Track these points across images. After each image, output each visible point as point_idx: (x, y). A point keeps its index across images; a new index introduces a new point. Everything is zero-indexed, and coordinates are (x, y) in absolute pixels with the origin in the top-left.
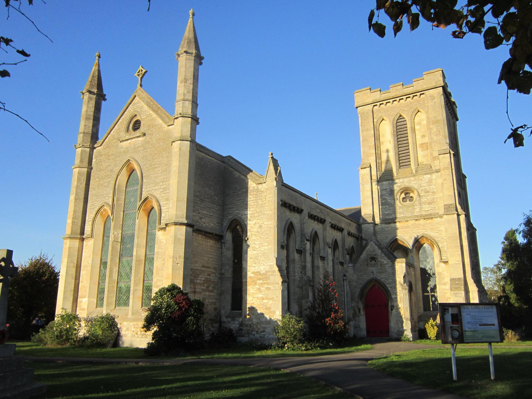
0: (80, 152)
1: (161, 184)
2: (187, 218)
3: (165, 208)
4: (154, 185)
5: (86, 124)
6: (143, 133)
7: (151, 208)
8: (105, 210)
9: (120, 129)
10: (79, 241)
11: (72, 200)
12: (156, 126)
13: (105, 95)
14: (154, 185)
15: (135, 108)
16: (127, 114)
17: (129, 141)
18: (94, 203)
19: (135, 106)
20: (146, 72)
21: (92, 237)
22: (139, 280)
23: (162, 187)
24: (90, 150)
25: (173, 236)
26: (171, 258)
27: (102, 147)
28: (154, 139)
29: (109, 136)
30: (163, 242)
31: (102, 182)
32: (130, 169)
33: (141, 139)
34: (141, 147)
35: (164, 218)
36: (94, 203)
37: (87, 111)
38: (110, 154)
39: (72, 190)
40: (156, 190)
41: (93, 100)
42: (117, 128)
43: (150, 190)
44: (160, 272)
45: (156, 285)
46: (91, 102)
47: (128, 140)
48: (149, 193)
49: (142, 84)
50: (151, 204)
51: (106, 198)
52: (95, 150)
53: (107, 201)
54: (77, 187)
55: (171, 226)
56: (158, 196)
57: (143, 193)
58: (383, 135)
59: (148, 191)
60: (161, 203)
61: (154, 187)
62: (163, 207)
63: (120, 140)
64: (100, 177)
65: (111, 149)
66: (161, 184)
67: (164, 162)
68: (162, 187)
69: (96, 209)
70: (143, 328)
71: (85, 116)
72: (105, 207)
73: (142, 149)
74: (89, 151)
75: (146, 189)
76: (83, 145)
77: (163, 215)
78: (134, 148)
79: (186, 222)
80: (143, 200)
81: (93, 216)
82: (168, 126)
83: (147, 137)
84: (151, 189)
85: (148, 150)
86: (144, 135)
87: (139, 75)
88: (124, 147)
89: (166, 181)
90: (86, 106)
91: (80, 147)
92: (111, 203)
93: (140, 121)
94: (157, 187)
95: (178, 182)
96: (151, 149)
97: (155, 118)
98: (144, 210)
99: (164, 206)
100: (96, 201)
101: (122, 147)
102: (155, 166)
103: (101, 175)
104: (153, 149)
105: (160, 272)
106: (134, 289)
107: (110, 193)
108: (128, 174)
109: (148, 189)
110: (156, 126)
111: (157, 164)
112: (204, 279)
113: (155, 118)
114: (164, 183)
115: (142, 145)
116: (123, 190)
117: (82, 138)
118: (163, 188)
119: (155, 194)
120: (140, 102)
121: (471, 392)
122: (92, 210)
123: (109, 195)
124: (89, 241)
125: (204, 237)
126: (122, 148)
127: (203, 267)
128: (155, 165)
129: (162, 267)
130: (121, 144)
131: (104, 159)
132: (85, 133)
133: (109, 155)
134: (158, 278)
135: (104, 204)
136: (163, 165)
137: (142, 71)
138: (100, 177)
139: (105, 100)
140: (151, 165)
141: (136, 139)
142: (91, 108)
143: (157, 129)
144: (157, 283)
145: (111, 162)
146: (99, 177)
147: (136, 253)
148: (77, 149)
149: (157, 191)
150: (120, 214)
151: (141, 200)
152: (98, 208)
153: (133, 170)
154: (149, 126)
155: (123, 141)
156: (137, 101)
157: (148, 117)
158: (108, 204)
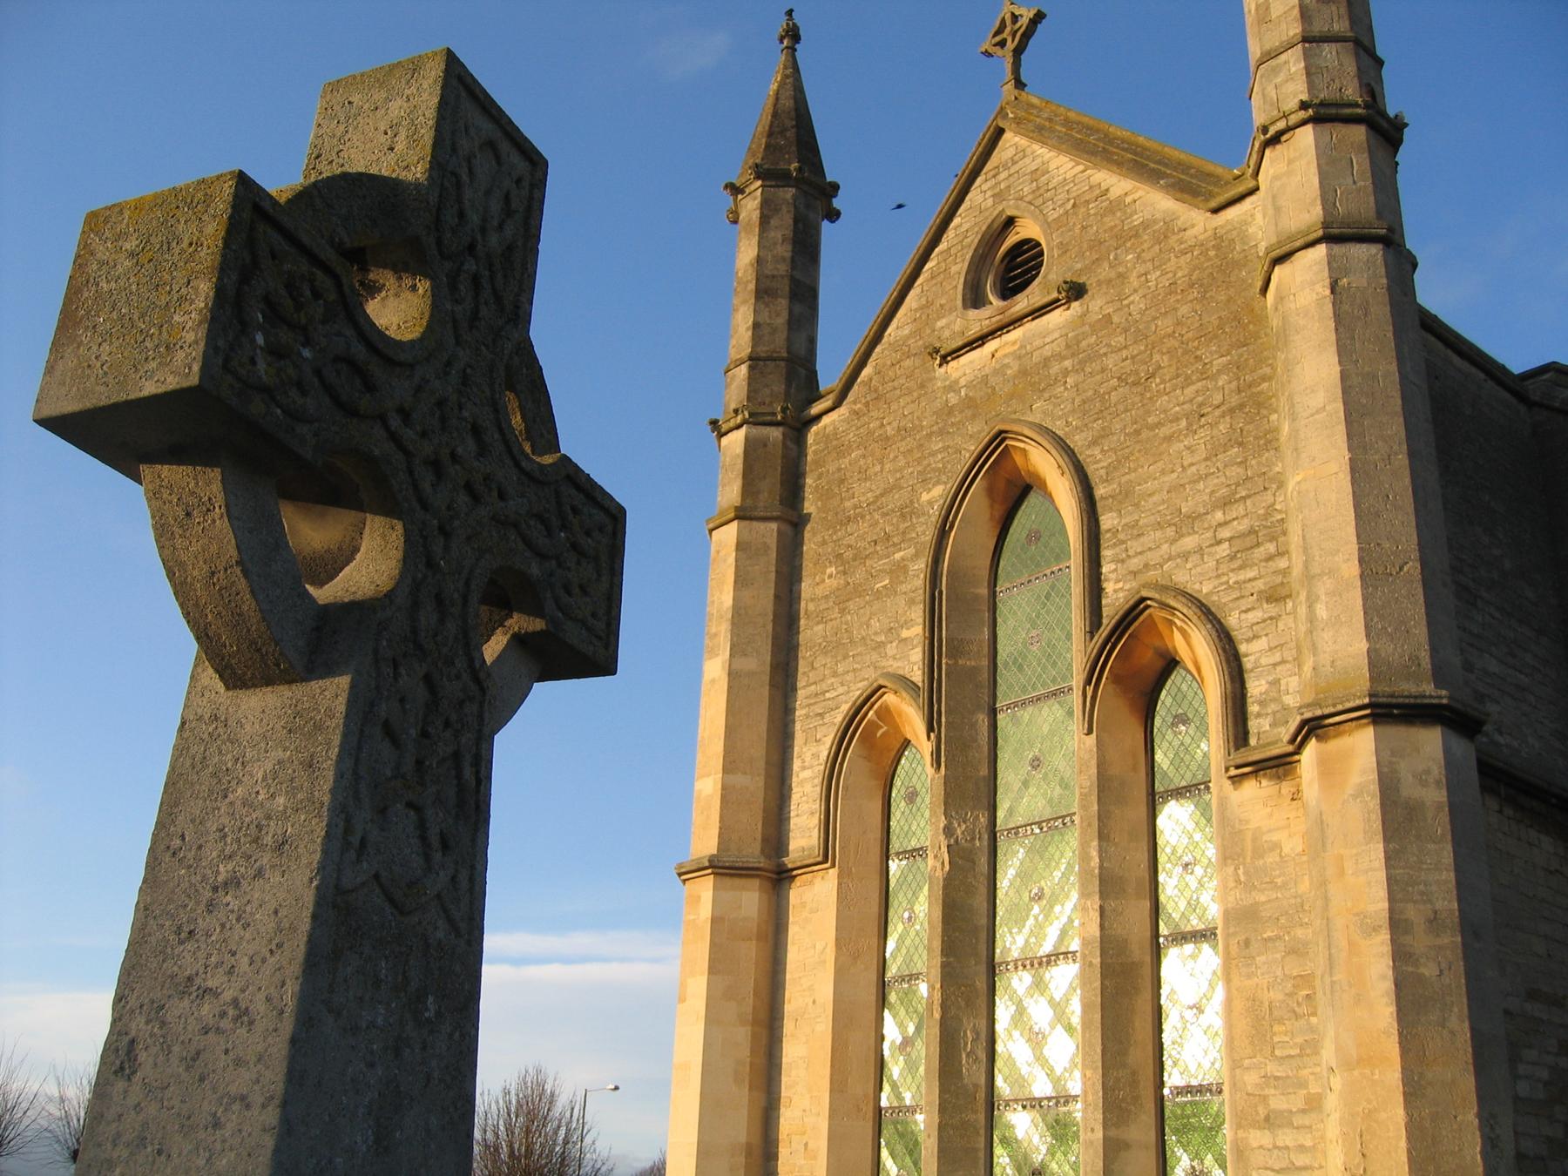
0: (739, 449)
1: (1219, 516)
2: (1439, 675)
3: (1262, 644)
4: (1170, 532)
5: (760, 320)
6: (1065, 282)
7: (1159, 664)
8: (886, 714)
9: (929, 304)
10: (1314, 129)
11: (713, 681)
12: (1137, 235)
13: (835, 187)
14: (1170, 532)
15: (1003, 186)
16: (960, 225)
17: (991, 346)
18: (824, 686)
19: (1003, 175)
20: (1039, 17)
21: (825, 860)
22: (1134, 1083)
23: (1225, 533)
24: (784, 434)
25: (1375, 788)
26: (1376, 929)
27: (843, 410)
28: (1136, 297)
29: (878, 349)
30: (1277, 846)
31: (859, 575)
32: (1009, 482)
33: (1056, 318)
34: (1064, 358)
35: (1262, 703)
36: (824, 686)
37: (759, 260)
38: (890, 431)
39: (714, 630)
40: (1185, 556)
41: (784, 209)
42: (915, 306)
43: (1146, 566)
44: (1276, 1028)
45: (1262, 1112)
46: (773, 222)
47: (981, 340)
48: (1143, 578)
49: (1023, 79)
50: (1158, 643)
51: (891, 649)
52: (813, 432)
53: (895, 666)
54: (739, 615)
55: (1350, 732)
56: (1204, 589)
57: (1109, 587)
58: (1162, 832)
59: (1135, 574)
60: (1232, 621)
61: (1173, 542)
62: (1249, 640)
63: (942, 352)
64: (849, 554)
65: (894, 406)
66: (1219, 516)
67: (1217, 399)
68: (1225, 533)
69: (839, 717)
70: (538, 1072)
71: (752, 286)
72: (889, 698)
73: (1067, 363)
74: (781, 437)
75: (1123, 561)
76: (751, 415)
77: (1256, 687)
78: (1023, 372)
79: (1442, 696)
80: (1104, 632)
81: (824, 749)
82: (1216, 211)
83: (1095, 304)
84: (1153, 557)
85: (1110, 362)
86: (1076, 291)
87: (1002, 44)
88: (963, 382)
89: (1244, 498)
90: (755, 240)
91: (738, 427)
92: (917, 676)
93: (1039, 244)
94: (1189, 542)
95: (1355, 470)
96: (1124, 353)
97: (1128, 200)
98: (1116, 679)
99: (1256, 637)
100: (835, 674)
101: (956, 382)
102: (1164, 431)
103: (851, 540)
104: (1134, 350)
105: (1276, 1028)
106: (1105, 1138)
107: (907, 624)
108: (999, 511)
109: (1135, 563)
110: (1137, 235)
111: (1177, 419)
112: (1545, 1075)
113: (1128, 200)
114: (1238, 510)
115: (1068, 346)
116: (976, 597)
117: (745, 384)
118: (1230, 539)
119: (1181, 578)
120: (1028, 151)
121: (549, 1091)
122: (817, 722)
123: (905, 634)
124: (811, 883)
125: (1509, 812)
126: (953, 387)
127: (1533, 995)
128: (1159, 425)
129: (1290, 995)
130: (942, 370)
131: (862, 462)
132: (759, 359)
133: (887, 438)
134: (1272, 1068)
135: (882, 682)
136: (1217, 412)
137: (1015, 18)
138: (849, 554)
139: (833, 215)
140: (1137, 432)
141: (1030, 327)
142: (775, 244)
143: (1145, 246)
144: (1265, 1098)
145: (900, 470)
146: (839, 556)
147: (1102, 926)
148: (724, 440)
149: (1194, 559)
150: (973, 726)
151: (1100, 624)
152: (845, 708)
153: (1026, 490)
154: (1097, 243)
155: (956, 353)
156: (1010, 153)
157: (1087, 202)
158: (905, 682)
